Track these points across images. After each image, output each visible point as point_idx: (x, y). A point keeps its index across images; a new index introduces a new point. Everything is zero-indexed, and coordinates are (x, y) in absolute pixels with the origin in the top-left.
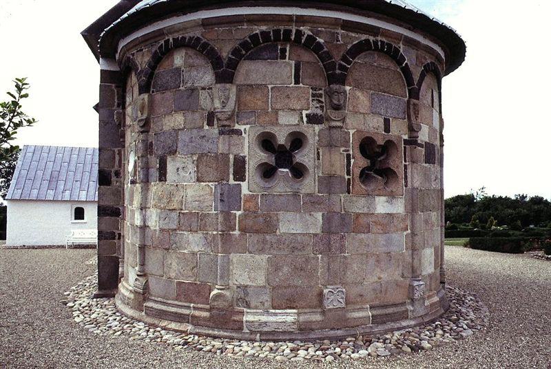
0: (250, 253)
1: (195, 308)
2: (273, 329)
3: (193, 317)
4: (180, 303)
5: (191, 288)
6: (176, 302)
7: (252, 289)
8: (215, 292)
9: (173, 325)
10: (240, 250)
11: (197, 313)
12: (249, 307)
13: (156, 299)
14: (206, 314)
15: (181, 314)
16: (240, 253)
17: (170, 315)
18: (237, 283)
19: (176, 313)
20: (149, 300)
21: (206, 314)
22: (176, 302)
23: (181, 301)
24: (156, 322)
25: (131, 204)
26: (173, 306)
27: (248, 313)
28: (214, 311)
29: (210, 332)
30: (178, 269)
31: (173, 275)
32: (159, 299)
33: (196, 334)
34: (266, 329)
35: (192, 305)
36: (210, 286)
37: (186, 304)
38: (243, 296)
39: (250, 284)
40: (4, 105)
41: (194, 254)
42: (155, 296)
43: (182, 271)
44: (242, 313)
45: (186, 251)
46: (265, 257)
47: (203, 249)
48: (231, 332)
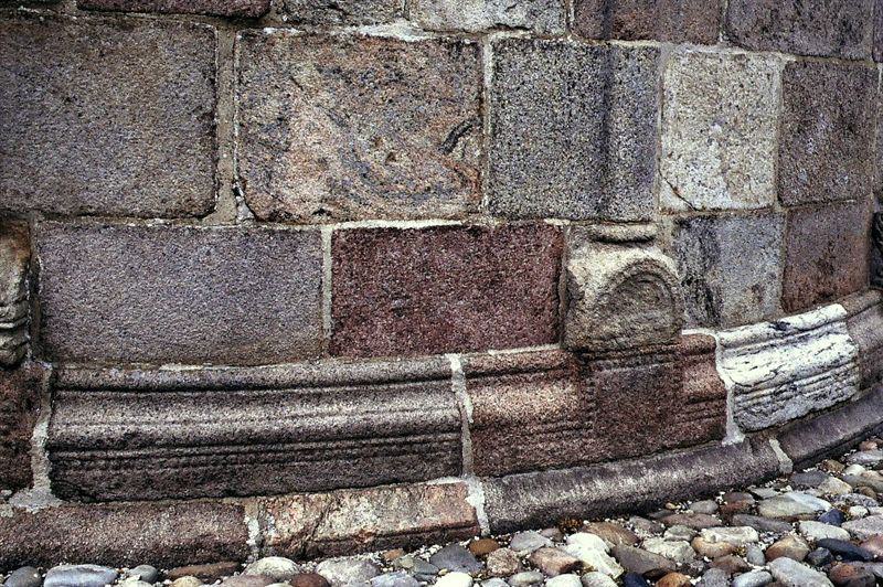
0: (734, 41)
1: (475, 377)
2: (811, 404)
3: (486, 427)
4: (375, 368)
5: (445, 258)
6: (332, 368)
7: (730, 226)
8: (399, 30)
9: (358, 514)
10: (695, 29)
11: (501, 401)
12: (714, 319)
13: (142, 376)
14: (549, 398)
15: (408, 430)
16: (696, 41)
17: (322, 455)
18: (678, 204)
19: (364, 434)
20: (60, 393)
21: (549, 398)
22: (332, 368)
23: (367, 353)
24: (208, 525)
25: (730, 533)
26: (317, 391)
27: (726, 347)
28: (610, 372)
29: (601, 487)
30: (351, 156)
31: (303, 192)
32: (174, 372)
33: (537, 521)
34: (794, 410)
35: (455, 362)
36: (559, 233)
37: (419, 364)
38: (698, 268)
39: (723, 201)
40: (4, 421)
41: (456, 44)
42: (125, 362)
43: (373, 158)
44: (707, 352)
45: (399, 30)
46: (776, 62)
47: (519, 16)
48: (686, 463)
